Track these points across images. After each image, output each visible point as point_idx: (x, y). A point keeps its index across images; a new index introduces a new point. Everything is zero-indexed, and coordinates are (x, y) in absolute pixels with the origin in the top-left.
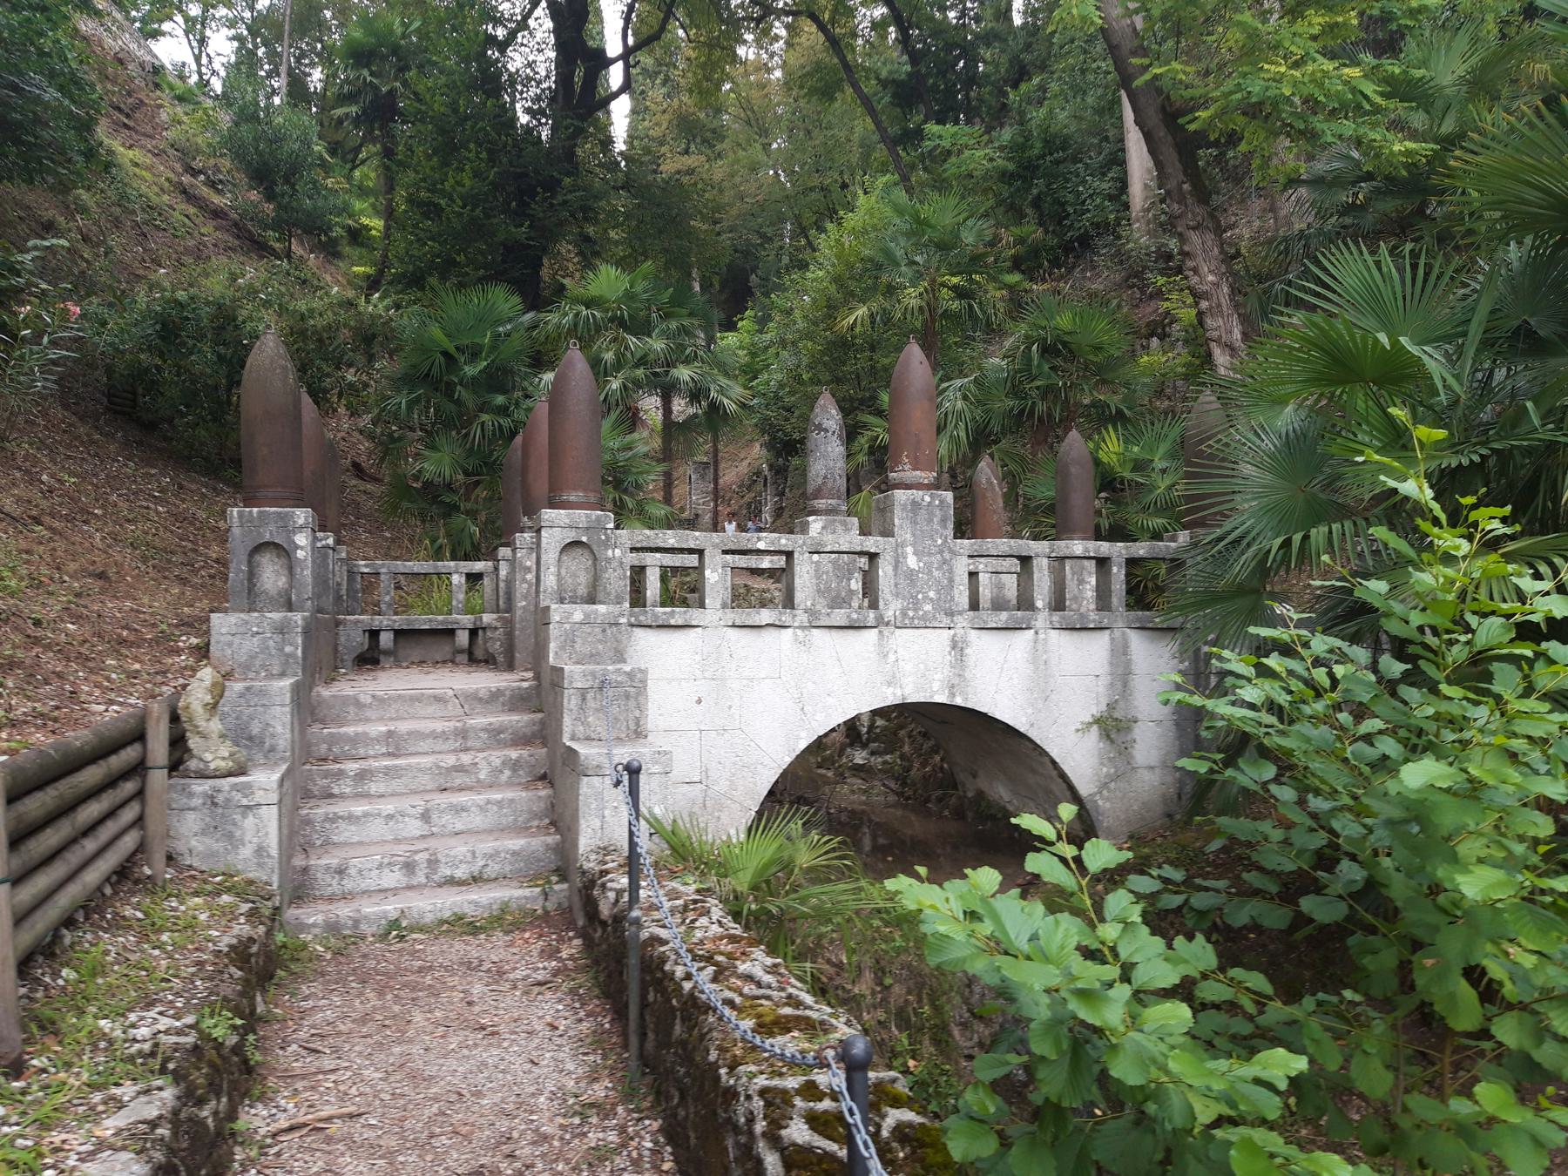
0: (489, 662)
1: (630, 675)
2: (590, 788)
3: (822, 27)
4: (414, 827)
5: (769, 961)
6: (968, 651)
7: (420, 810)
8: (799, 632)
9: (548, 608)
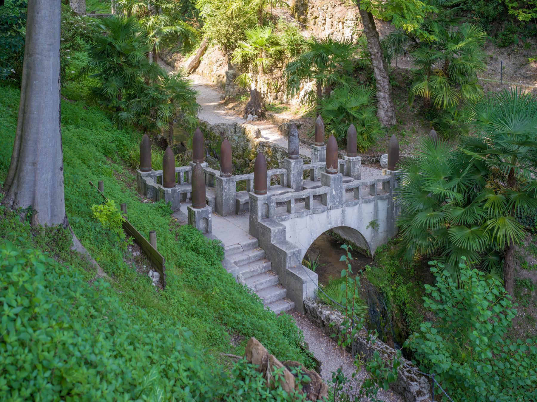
1: (298, 251)
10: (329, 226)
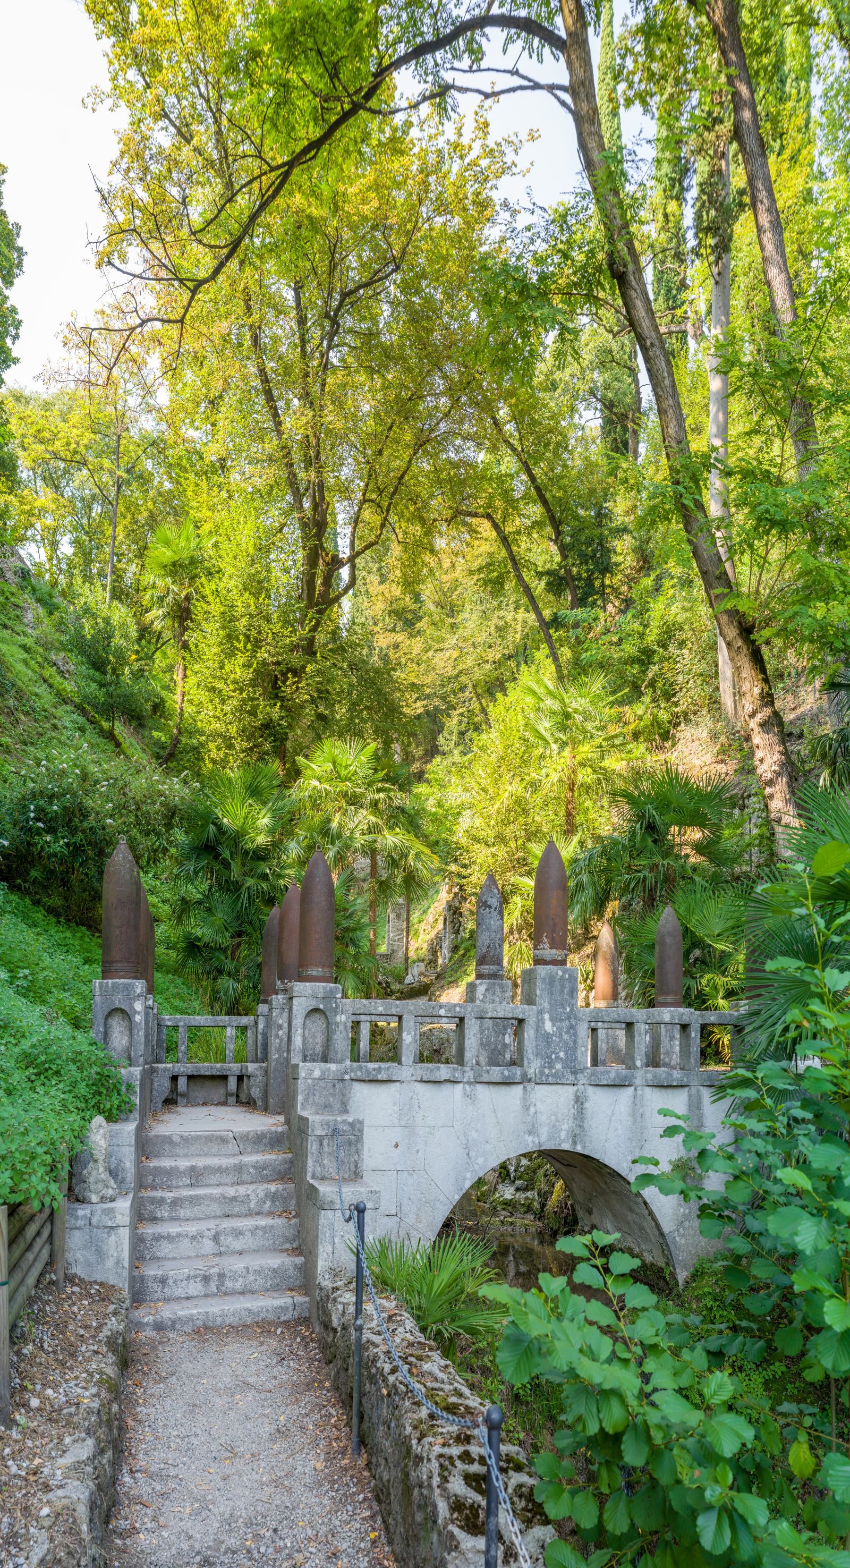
0: (249, 1104)
1: (352, 1125)
2: (326, 1218)
3: (496, 526)
4: (208, 1246)
5: (443, 1363)
6: (587, 1105)
7: (213, 1232)
8: (467, 1087)
9: (297, 1066)
10: (530, 1139)
